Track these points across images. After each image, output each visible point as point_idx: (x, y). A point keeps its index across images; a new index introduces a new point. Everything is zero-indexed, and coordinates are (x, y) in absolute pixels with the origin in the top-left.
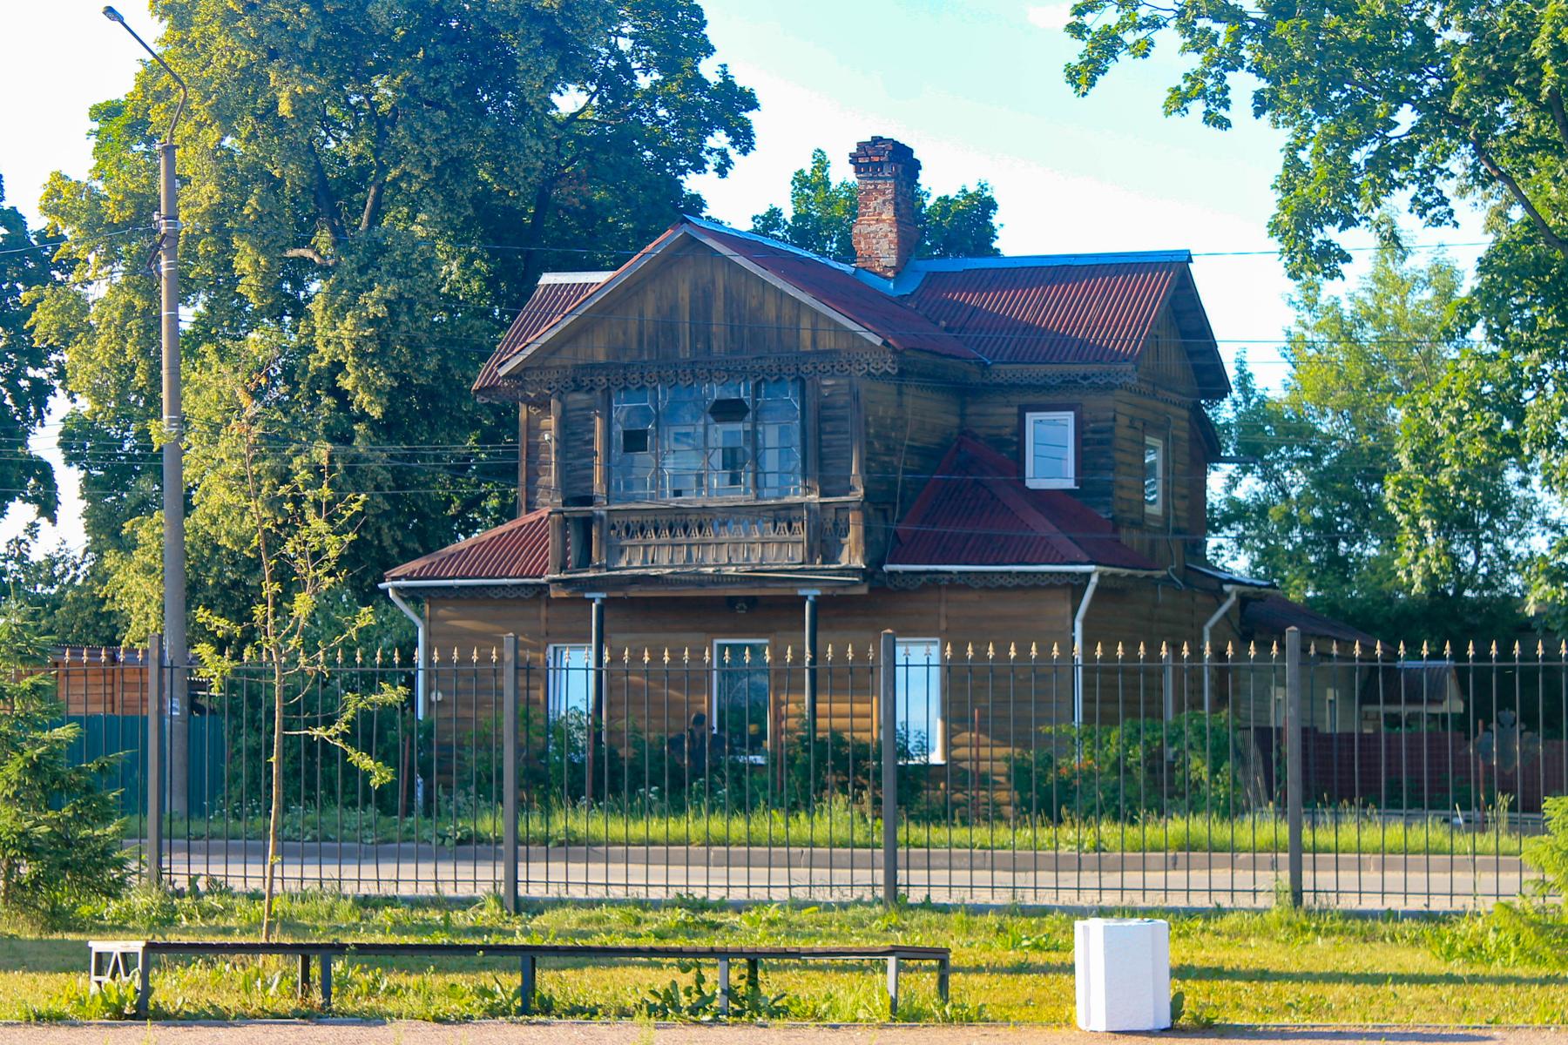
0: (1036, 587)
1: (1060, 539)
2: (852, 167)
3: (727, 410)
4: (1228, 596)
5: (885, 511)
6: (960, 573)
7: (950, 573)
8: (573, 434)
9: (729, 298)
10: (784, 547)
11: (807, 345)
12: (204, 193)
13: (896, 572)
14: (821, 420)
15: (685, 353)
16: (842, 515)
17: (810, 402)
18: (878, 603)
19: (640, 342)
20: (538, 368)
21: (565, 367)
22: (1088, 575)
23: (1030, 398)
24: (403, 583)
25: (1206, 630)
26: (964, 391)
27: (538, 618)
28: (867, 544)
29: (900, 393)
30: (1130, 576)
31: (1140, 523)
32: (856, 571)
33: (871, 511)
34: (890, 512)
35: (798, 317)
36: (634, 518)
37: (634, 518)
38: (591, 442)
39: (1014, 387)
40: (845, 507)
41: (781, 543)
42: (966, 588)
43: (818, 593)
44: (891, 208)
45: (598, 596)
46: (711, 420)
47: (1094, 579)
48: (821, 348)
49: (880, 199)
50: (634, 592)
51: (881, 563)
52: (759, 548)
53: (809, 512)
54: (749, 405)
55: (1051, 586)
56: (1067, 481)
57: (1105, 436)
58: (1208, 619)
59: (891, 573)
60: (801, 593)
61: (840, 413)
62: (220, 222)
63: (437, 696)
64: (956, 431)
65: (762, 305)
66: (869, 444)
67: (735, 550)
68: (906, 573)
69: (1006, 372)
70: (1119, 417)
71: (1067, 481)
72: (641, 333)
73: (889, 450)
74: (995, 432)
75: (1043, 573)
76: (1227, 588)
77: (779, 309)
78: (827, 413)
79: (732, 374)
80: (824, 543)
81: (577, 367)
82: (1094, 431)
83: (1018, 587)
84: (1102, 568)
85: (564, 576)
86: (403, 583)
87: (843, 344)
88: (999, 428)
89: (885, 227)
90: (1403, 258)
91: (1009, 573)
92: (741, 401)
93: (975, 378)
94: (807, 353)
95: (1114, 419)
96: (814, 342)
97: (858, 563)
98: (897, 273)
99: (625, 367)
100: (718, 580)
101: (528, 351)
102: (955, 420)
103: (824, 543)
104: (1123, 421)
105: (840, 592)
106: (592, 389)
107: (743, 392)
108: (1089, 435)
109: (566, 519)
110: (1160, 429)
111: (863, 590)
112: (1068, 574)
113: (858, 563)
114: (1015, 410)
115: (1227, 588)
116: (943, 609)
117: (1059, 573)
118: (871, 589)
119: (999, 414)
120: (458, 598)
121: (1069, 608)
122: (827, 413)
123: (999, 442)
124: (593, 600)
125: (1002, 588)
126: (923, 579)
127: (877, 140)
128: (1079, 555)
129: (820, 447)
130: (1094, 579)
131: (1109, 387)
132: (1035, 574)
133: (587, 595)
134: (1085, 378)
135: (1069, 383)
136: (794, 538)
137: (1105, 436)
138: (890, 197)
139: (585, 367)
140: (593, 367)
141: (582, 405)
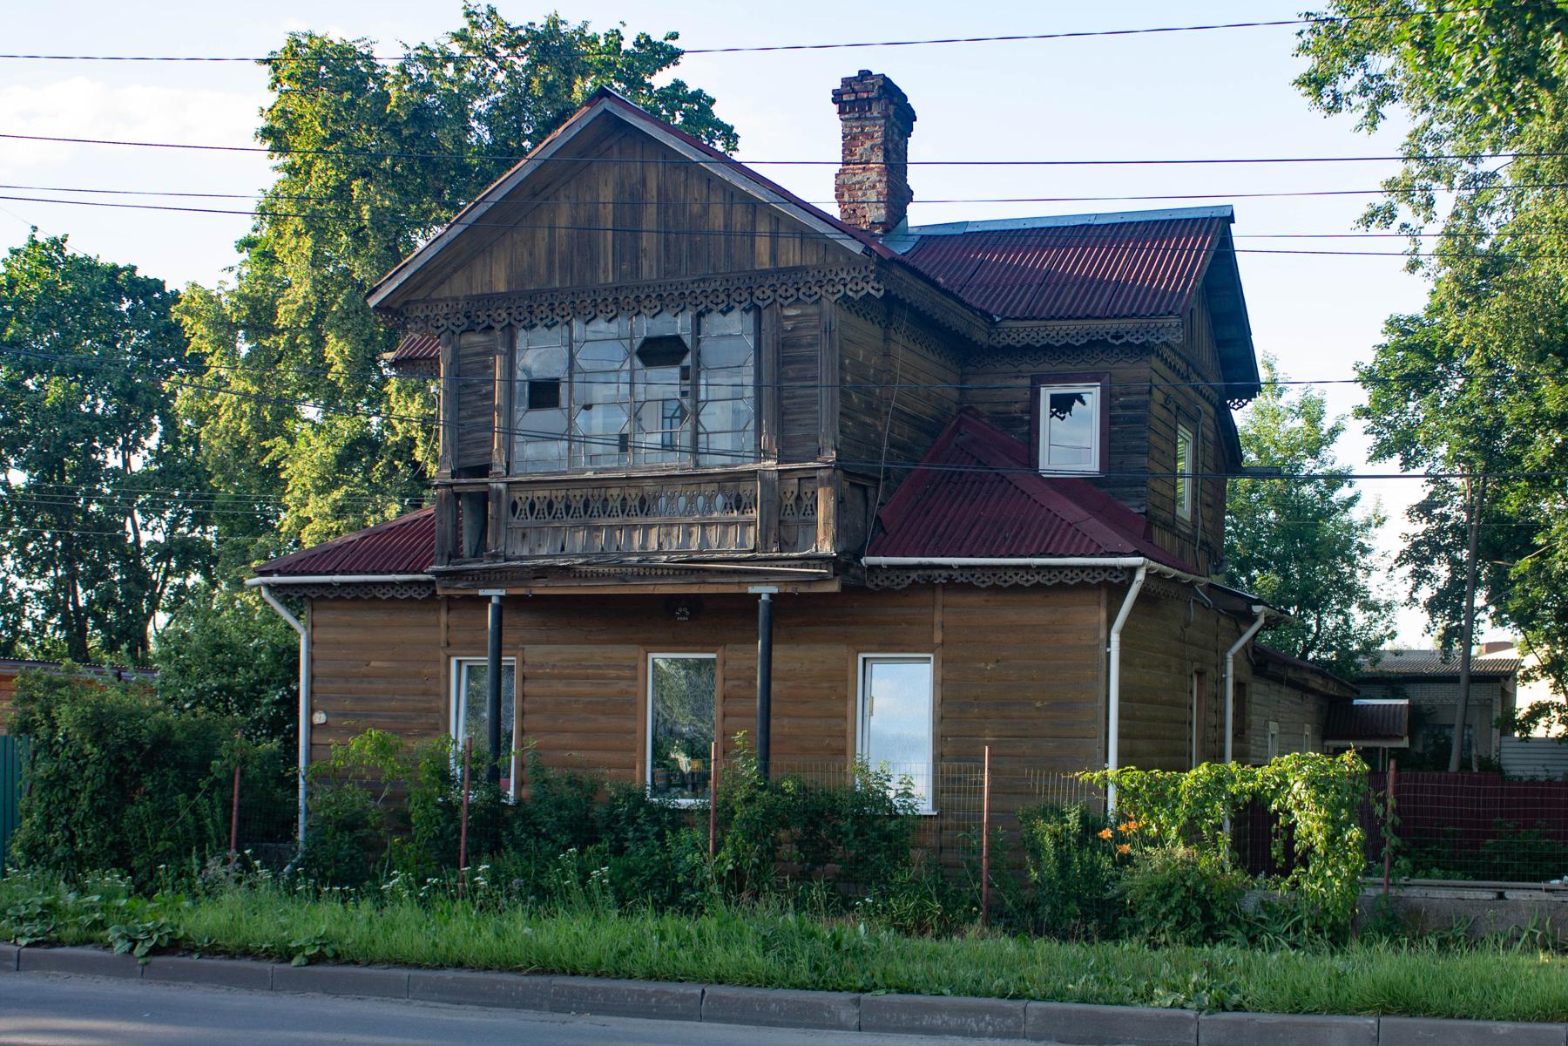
0: (1061, 587)
1: (1095, 527)
2: (835, 108)
3: (658, 351)
4: (1253, 619)
5: (865, 488)
6: (962, 567)
7: (949, 567)
8: (466, 386)
9: (665, 202)
10: (732, 530)
11: (764, 261)
12: (301, 291)
13: (879, 566)
14: (782, 362)
15: (607, 277)
16: (808, 487)
17: (767, 339)
18: (860, 606)
19: (551, 263)
20: (424, 301)
21: (456, 299)
22: (1132, 570)
23: (1046, 367)
24: (276, 579)
25: (1230, 656)
26: (964, 351)
27: (438, 626)
28: (838, 526)
29: (887, 339)
30: (1175, 579)
31: (1171, 525)
32: (824, 560)
33: (846, 485)
34: (871, 492)
35: (754, 223)
36: (540, 493)
37: (540, 493)
38: (490, 395)
39: (1027, 351)
40: (808, 477)
41: (728, 525)
42: (968, 588)
43: (775, 590)
44: (881, 154)
45: (495, 593)
46: (638, 363)
47: (1140, 576)
48: (782, 265)
49: (868, 144)
50: (540, 589)
51: (858, 556)
52: (697, 531)
53: (765, 483)
54: (688, 340)
55: (1083, 586)
56: (1091, 464)
57: (1139, 412)
58: (1231, 646)
59: (872, 568)
60: (752, 590)
61: (806, 352)
62: (317, 321)
63: (320, 718)
64: (954, 409)
65: (706, 209)
66: (844, 394)
67: (668, 534)
68: (891, 567)
69: (1019, 332)
70: (1155, 390)
71: (1091, 464)
72: (551, 251)
73: (872, 410)
74: (1000, 408)
75: (1072, 568)
76: (1256, 609)
77: (728, 215)
78: (792, 352)
79: (665, 300)
80: (785, 520)
81: (470, 299)
82: (1124, 407)
83: (1038, 587)
84: (1153, 564)
85: (451, 568)
86: (276, 579)
87: (812, 259)
88: (1007, 403)
89: (874, 176)
90: (1279, 396)
91: (1027, 567)
92: (678, 338)
93: (980, 336)
94: (764, 273)
95: (1150, 392)
96: (774, 256)
97: (826, 548)
98: (887, 231)
99: (531, 296)
100: (647, 570)
101: (404, 276)
102: (955, 394)
103: (785, 520)
104: (1158, 396)
105: (803, 589)
106: (490, 328)
107: (679, 325)
108: (1119, 412)
109: (458, 496)
110: (1192, 420)
111: (834, 587)
112: (1105, 568)
113: (826, 548)
114: (1027, 382)
115: (1256, 609)
116: (938, 618)
117: (1094, 568)
118: (844, 587)
119: (1005, 385)
120: (339, 598)
121: (1103, 615)
122: (792, 352)
123: (1009, 422)
124: (489, 598)
125: (1017, 588)
126: (914, 575)
127: (865, 74)
128: (1122, 543)
129: (780, 398)
130: (1140, 576)
131: (1145, 349)
132: (1061, 568)
133: (481, 593)
134: (1117, 336)
135: (1097, 345)
136: (743, 518)
137: (1139, 412)
138: (879, 141)
139: (480, 297)
140: (490, 299)
141: (479, 349)
